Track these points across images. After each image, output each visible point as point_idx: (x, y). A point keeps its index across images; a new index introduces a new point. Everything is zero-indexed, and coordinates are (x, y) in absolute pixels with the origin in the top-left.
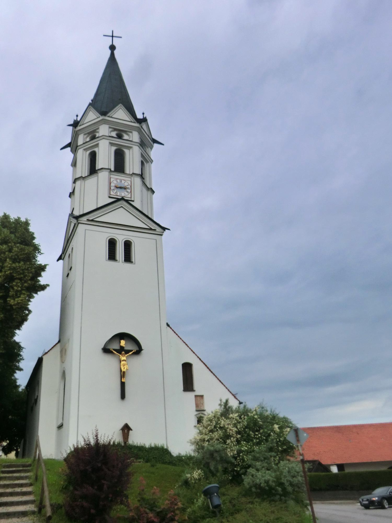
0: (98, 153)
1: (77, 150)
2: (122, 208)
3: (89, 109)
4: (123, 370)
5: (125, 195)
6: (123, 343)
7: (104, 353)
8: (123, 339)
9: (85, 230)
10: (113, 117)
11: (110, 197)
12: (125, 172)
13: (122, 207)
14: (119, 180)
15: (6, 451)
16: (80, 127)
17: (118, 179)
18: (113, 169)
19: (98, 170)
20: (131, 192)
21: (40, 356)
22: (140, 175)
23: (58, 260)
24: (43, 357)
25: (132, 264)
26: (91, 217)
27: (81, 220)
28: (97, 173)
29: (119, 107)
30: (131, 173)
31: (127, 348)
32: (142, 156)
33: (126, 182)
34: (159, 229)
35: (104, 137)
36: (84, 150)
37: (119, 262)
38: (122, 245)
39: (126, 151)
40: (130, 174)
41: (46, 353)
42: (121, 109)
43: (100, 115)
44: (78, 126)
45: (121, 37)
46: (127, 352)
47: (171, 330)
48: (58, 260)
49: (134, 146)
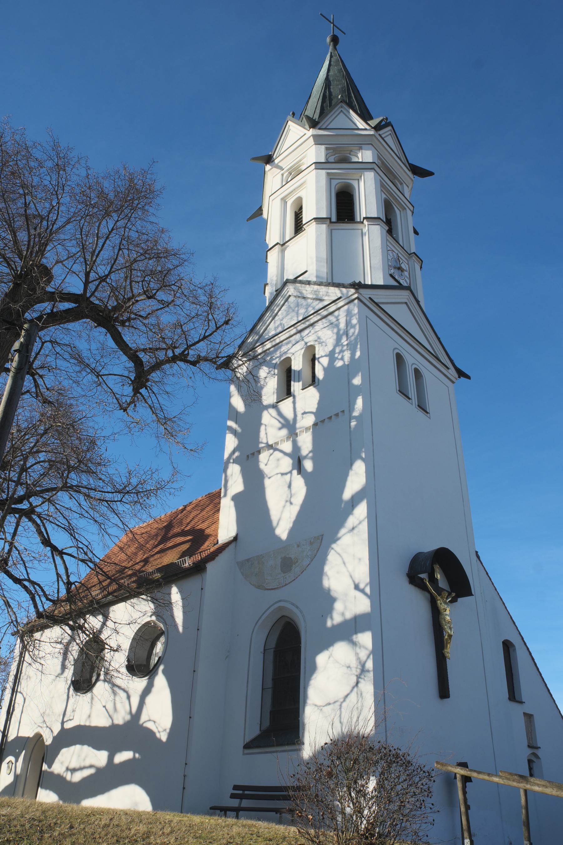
2: (405, 305)
13: (406, 303)
18: (334, 219)
34: (452, 373)
45: (345, 34)
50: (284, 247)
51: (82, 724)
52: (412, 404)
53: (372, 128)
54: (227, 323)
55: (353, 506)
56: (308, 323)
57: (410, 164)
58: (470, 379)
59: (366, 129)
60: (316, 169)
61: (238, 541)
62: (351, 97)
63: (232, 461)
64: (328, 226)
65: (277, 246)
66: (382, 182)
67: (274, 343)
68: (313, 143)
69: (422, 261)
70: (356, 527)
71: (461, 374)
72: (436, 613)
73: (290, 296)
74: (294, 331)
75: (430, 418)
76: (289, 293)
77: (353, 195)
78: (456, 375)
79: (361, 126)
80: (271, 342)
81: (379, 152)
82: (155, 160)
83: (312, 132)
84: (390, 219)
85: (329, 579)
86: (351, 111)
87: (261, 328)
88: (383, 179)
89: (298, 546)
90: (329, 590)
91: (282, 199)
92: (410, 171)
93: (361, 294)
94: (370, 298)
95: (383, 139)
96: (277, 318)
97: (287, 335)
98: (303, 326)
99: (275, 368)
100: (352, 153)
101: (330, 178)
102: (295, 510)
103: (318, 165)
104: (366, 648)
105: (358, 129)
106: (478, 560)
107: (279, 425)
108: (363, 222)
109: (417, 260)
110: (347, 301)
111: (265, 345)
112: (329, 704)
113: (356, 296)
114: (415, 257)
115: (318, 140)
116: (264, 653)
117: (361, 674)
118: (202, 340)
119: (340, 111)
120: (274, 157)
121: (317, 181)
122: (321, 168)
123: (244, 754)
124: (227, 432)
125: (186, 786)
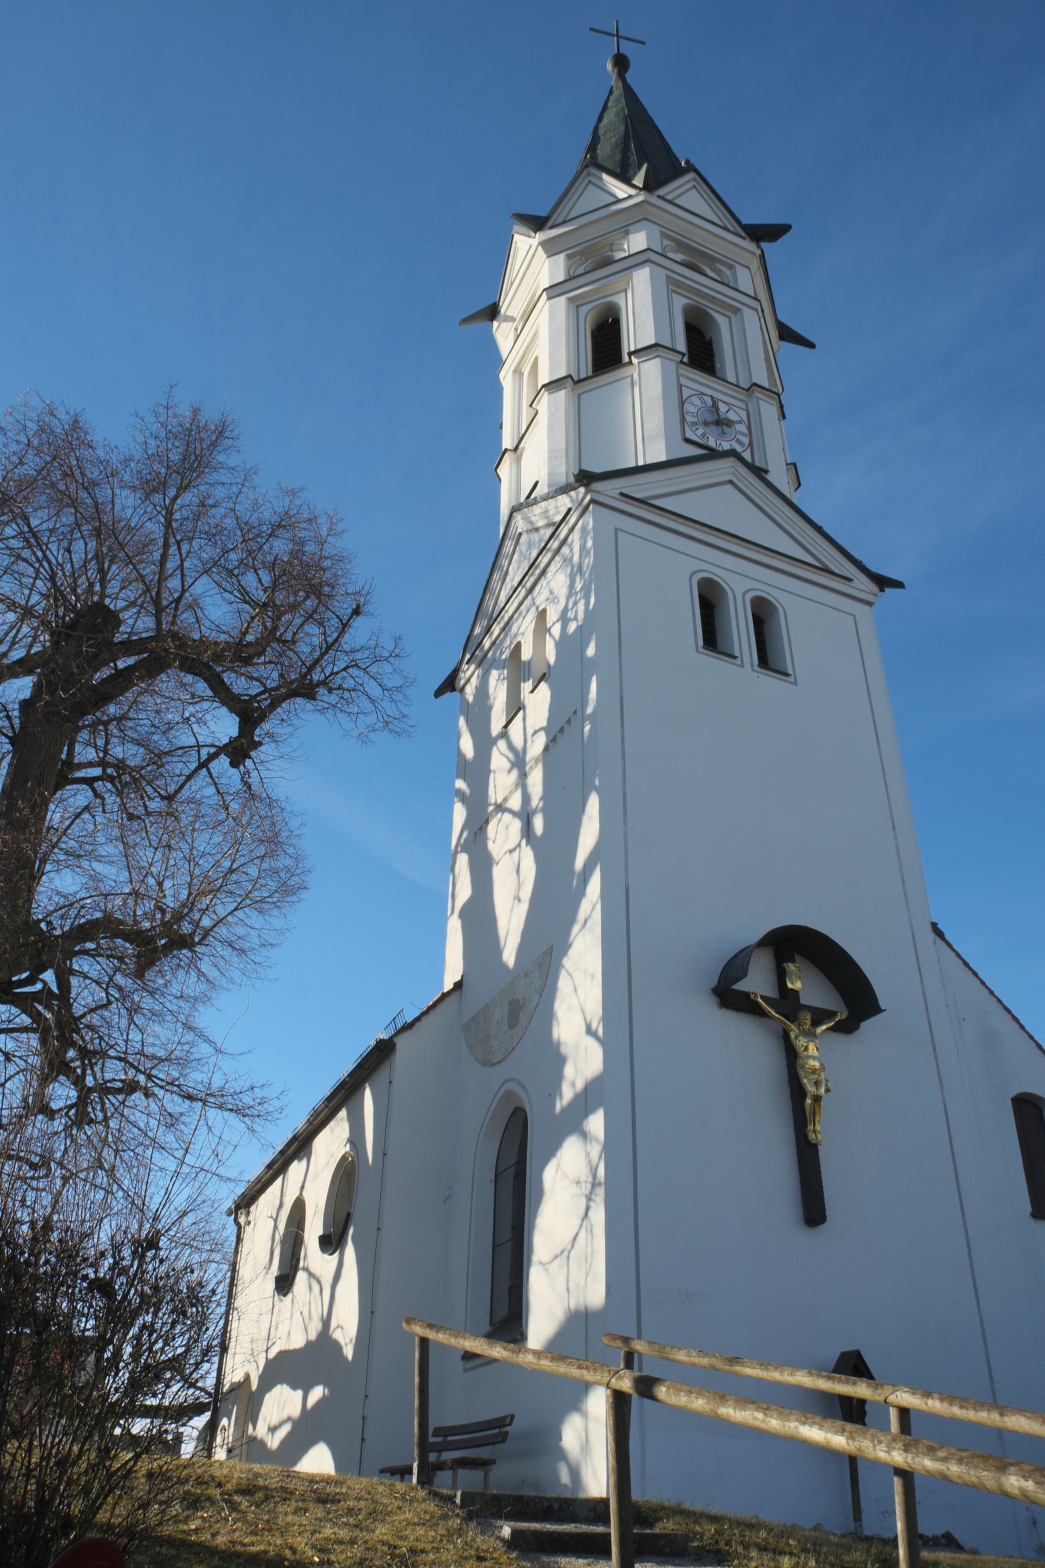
2: (729, 487)
3: (584, 179)
9: (616, 530)
10: (677, 201)
13: (731, 482)
21: (385, 1036)
23: (438, 693)
24: (395, 1040)
26: (636, 486)
33: (731, 411)
34: (863, 584)
41: (408, 1027)
42: (694, 190)
45: (644, 43)
47: (953, 954)
48: (438, 693)
49: (746, 311)
50: (519, 451)
51: (283, 1349)
52: (742, 666)
53: (641, 189)
54: (357, 612)
55: (585, 880)
56: (538, 572)
57: (744, 227)
59: (630, 197)
60: (549, 298)
61: (463, 988)
62: (629, 150)
63: (459, 849)
64: (573, 390)
65: (506, 455)
67: (502, 624)
68: (545, 256)
70: (589, 917)
71: (883, 582)
72: (792, 1055)
73: (520, 534)
74: (523, 592)
75: (795, 683)
76: (519, 530)
78: (872, 587)
79: (621, 195)
80: (499, 623)
81: (662, 227)
82: (173, 384)
83: (540, 236)
84: (711, 339)
85: (558, 1024)
86: (606, 177)
87: (489, 603)
89: (526, 975)
90: (559, 1043)
91: (515, 371)
92: (744, 238)
93: (598, 492)
94: (622, 494)
95: (671, 202)
96: (508, 578)
97: (516, 604)
98: (532, 579)
99: (504, 668)
100: (614, 247)
101: (575, 304)
102: (524, 908)
103: (550, 291)
104: (597, 1141)
105: (619, 201)
106: (939, 941)
107: (508, 765)
108: (630, 363)
109: (764, 394)
110: (580, 509)
111: (492, 633)
112: (556, 1257)
113: (588, 498)
114: (760, 392)
115: (550, 248)
116: (496, 1182)
117: (591, 1193)
118: (326, 652)
119: (586, 181)
120: (501, 304)
121: (552, 319)
122: (554, 294)
123: (466, 1370)
124: (456, 800)
125: (366, 1437)
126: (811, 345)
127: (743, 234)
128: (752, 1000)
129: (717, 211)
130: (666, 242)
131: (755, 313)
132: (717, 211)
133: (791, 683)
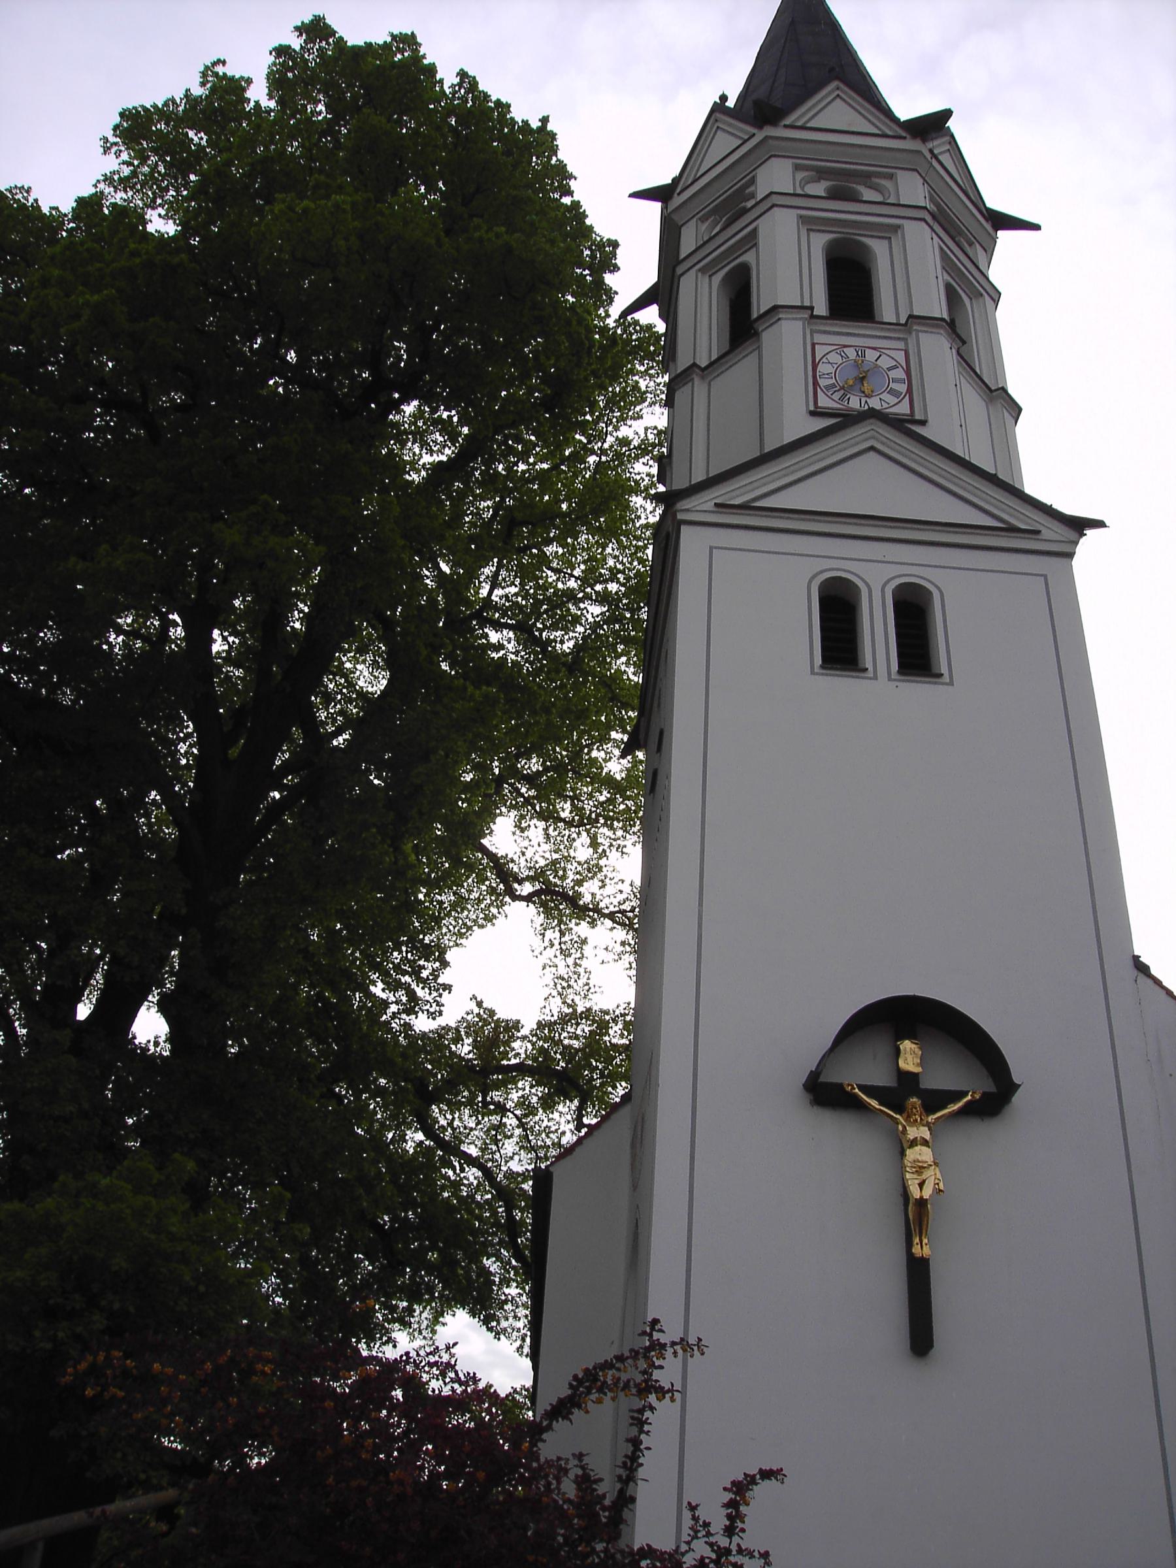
0: (758, 270)
1: (676, 280)
2: (872, 454)
4: (915, 1193)
5: (885, 405)
6: (910, 1057)
7: (817, 1110)
8: (912, 1036)
9: (711, 548)
11: (813, 414)
12: (877, 319)
13: (872, 448)
14: (852, 349)
15: (4, 476)
16: (681, 195)
17: (845, 346)
18: (821, 309)
19: (761, 317)
20: (910, 390)
22: (943, 320)
25: (936, 683)
26: (737, 491)
27: (687, 510)
28: (754, 339)
29: (830, 93)
30: (903, 321)
31: (939, 1079)
32: (948, 264)
33: (883, 356)
34: (1053, 532)
35: (775, 199)
36: (703, 270)
37: (875, 678)
38: (885, 624)
39: (879, 248)
40: (902, 325)
42: (838, 100)
43: (753, 130)
44: (676, 195)
46: (934, 1101)
58: (548, 116)
66: (946, 253)
69: (772, 193)
77: (870, 270)
88: (942, 241)
109: (924, 325)
114: (919, 324)
126: (1036, 227)
127: (904, 134)
128: (847, 1093)
129: (870, 117)
130: (800, 175)
131: (923, 224)
132: (870, 117)
133: (870, 679)
